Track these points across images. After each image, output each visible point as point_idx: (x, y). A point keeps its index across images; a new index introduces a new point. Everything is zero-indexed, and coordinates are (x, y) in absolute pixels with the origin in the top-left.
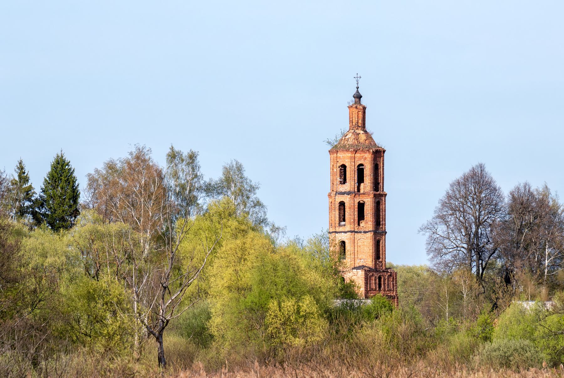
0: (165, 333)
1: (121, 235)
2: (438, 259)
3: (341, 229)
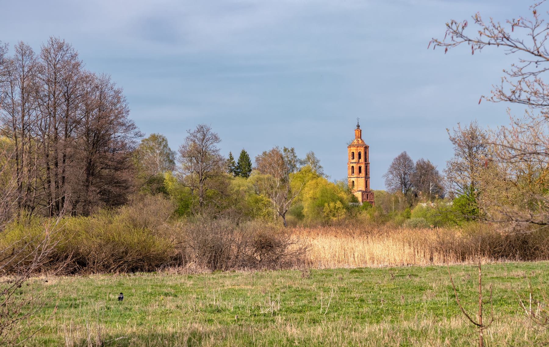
0: (286, 215)
1: (268, 179)
2: (389, 188)
3: (352, 176)
